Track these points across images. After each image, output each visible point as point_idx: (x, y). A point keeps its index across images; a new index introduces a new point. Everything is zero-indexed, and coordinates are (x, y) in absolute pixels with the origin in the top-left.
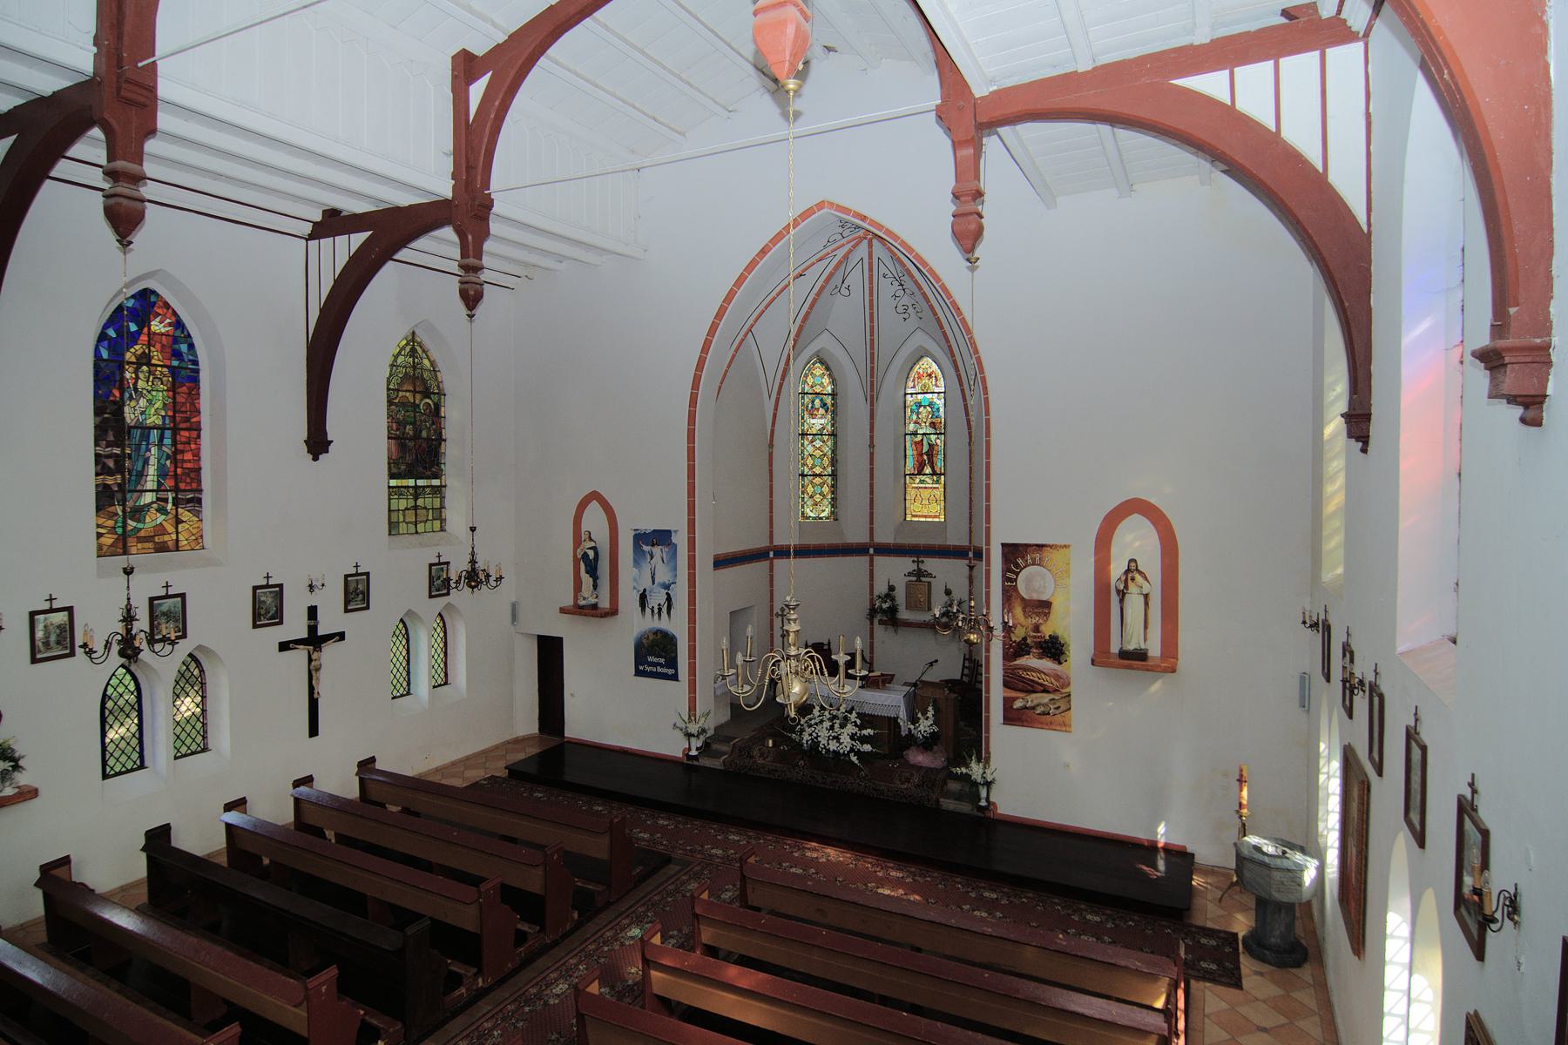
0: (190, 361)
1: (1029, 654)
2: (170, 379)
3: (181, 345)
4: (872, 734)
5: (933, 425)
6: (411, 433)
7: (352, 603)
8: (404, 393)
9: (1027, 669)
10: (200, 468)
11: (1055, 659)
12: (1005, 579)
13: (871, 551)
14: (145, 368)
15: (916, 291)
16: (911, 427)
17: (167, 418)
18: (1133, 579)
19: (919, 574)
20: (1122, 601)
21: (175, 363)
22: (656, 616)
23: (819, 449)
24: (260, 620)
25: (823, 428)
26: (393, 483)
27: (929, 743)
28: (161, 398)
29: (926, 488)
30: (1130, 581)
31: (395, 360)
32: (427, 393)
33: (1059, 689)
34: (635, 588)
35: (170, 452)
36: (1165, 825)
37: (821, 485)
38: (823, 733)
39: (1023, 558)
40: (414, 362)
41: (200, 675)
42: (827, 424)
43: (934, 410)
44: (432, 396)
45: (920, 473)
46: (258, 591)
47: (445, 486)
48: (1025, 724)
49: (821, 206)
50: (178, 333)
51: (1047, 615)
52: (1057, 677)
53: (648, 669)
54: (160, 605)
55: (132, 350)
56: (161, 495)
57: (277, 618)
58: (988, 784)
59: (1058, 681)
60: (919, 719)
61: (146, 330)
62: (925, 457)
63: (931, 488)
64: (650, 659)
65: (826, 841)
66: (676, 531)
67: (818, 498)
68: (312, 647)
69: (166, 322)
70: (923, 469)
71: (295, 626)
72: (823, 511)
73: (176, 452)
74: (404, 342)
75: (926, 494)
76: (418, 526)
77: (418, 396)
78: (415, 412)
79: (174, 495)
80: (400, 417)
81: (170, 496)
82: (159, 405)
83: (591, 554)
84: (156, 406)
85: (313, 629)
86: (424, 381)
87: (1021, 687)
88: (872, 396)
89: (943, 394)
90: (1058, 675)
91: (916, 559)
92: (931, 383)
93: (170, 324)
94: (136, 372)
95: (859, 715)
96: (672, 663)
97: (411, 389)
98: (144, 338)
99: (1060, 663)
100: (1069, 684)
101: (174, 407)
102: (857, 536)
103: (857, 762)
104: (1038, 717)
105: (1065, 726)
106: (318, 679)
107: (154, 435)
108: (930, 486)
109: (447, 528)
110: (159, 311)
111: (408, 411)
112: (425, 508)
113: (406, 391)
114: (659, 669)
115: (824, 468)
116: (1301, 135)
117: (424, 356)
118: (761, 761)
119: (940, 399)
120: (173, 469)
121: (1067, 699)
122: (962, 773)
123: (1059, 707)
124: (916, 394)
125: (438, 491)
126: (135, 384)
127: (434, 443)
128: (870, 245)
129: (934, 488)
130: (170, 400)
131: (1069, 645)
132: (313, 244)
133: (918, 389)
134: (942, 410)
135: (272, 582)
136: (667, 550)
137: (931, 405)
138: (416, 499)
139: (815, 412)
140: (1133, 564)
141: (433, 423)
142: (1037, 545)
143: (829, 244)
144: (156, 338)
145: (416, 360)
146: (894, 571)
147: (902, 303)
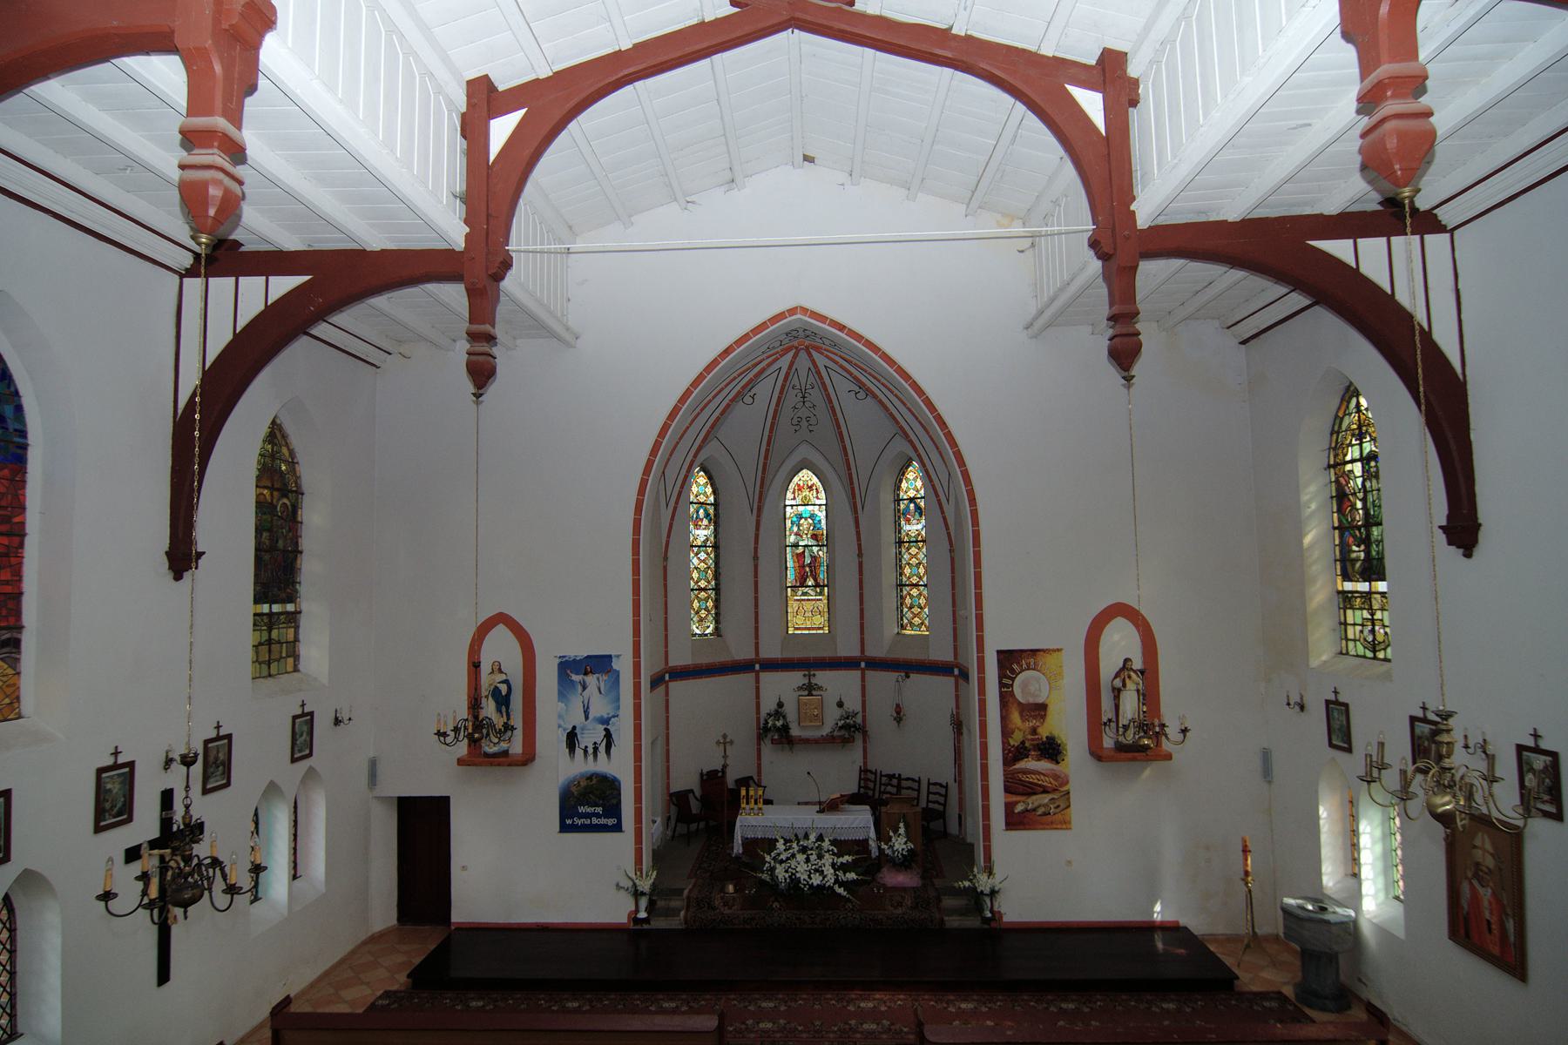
1: (1027, 757)
4: (850, 860)
5: (814, 537)
6: (267, 542)
7: (211, 780)
9: (1026, 772)
10: (21, 594)
11: (1053, 760)
12: (1002, 685)
13: (757, 667)
16: (792, 539)
19: (810, 688)
22: (591, 757)
23: (704, 561)
25: (707, 540)
27: (905, 863)
29: (808, 600)
32: (285, 492)
33: (1058, 788)
34: (559, 726)
36: (1161, 903)
37: (706, 600)
38: (802, 870)
39: (1018, 663)
41: (9, 918)
42: (710, 535)
43: (816, 522)
45: (802, 585)
46: (104, 775)
47: (300, 612)
48: (1027, 827)
49: (792, 311)
51: (1043, 717)
52: (1056, 777)
53: (579, 822)
57: (125, 813)
58: (993, 893)
59: (1056, 780)
60: (891, 837)
62: (807, 569)
63: (814, 600)
64: (581, 809)
65: (869, 986)
66: (618, 656)
67: (703, 613)
70: (805, 580)
71: (145, 825)
72: (708, 627)
75: (808, 606)
83: (503, 688)
87: (1021, 790)
89: (824, 507)
90: (1056, 775)
91: (807, 673)
92: (812, 495)
95: (834, 842)
96: (614, 810)
97: (270, 485)
99: (1058, 763)
100: (1067, 782)
102: (743, 652)
103: (845, 893)
104: (1039, 818)
105: (1065, 824)
108: (814, 597)
109: (301, 667)
111: (265, 514)
114: (595, 821)
115: (709, 582)
116: (1406, 296)
118: (727, 911)
119: (821, 511)
121: (1067, 796)
122: (964, 887)
123: (1058, 806)
124: (797, 505)
125: (293, 618)
127: (290, 555)
128: (810, 355)
129: (818, 600)
131: (1066, 745)
132: (193, 285)
133: (798, 501)
134: (823, 522)
135: (121, 760)
136: (605, 678)
137: (812, 516)
139: (700, 523)
141: (290, 530)
142: (1031, 650)
146: (781, 687)
147: (799, 414)
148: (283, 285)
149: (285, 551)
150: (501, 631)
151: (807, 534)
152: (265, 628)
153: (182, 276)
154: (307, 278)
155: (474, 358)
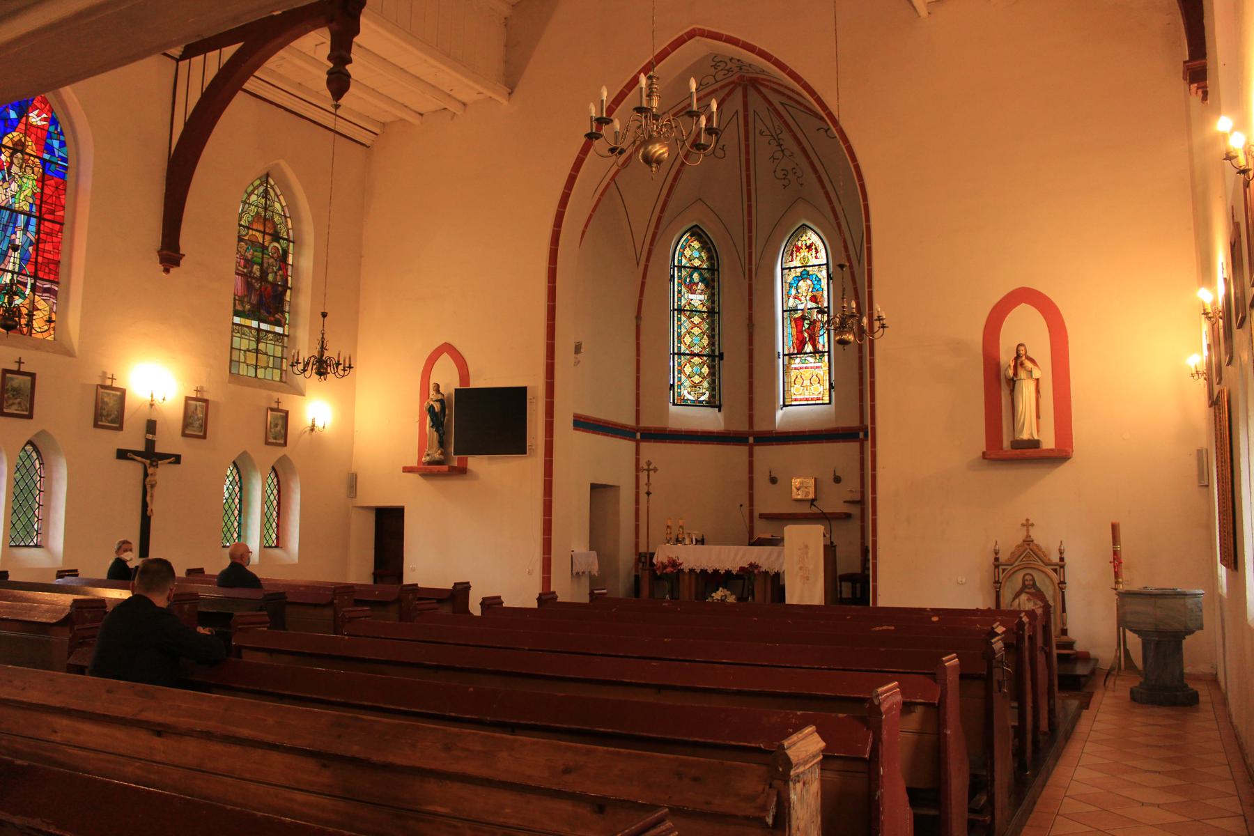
0: (60, 157)
2: (41, 170)
3: (54, 141)
8: (254, 232)
14: (19, 155)
15: (796, 149)
17: (34, 206)
18: (1022, 364)
20: (1012, 391)
21: (47, 156)
24: (101, 421)
26: (237, 320)
28: (30, 186)
29: (806, 368)
30: (1019, 367)
31: (248, 197)
35: (33, 240)
40: (266, 203)
44: (281, 241)
45: (801, 352)
49: (691, 35)
50: (52, 129)
54: (12, 379)
55: (10, 136)
56: (22, 278)
61: (24, 119)
62: (806, 335)
68: (148, 461)
69: (42, 116)
73: (38, 241)
74: (258, 182)
76: (258, 371)
77: (268, 238)
78: (263, 253)
79: (33, 281)
80: (249, 255)
81: (30, 281)
82: (28, 192)
84: (26, 193)
85: (150, 444)
86: (275, 225)
88: (750, 270)
89: (825, 266)
93: (45, 119)
94: (11, 156)
97: (263, 230)
98: (21, 126)
101: (42, 197)
106: (152, 496)
107: (22, 218)
110: (38, 105)
111: (256, 251)
112: (266, 354)
113: (257, 230)
117: (276, 200)
120: (35, 256)
126: (9, 169)
129: (817, 367)
130: (39, 190)
138: (258, 341)
140: (1022, 348)
141: (280, 269)
143: (701, 87)
144: (33, 129)
145: (268, 202)
148: (229, 51)
149: (274, 285)
150: (445, 359)
151: (805, 297)
152: (253, 339)
153: (178, 61)
154: (240, 44)
155: (1204, 452)
